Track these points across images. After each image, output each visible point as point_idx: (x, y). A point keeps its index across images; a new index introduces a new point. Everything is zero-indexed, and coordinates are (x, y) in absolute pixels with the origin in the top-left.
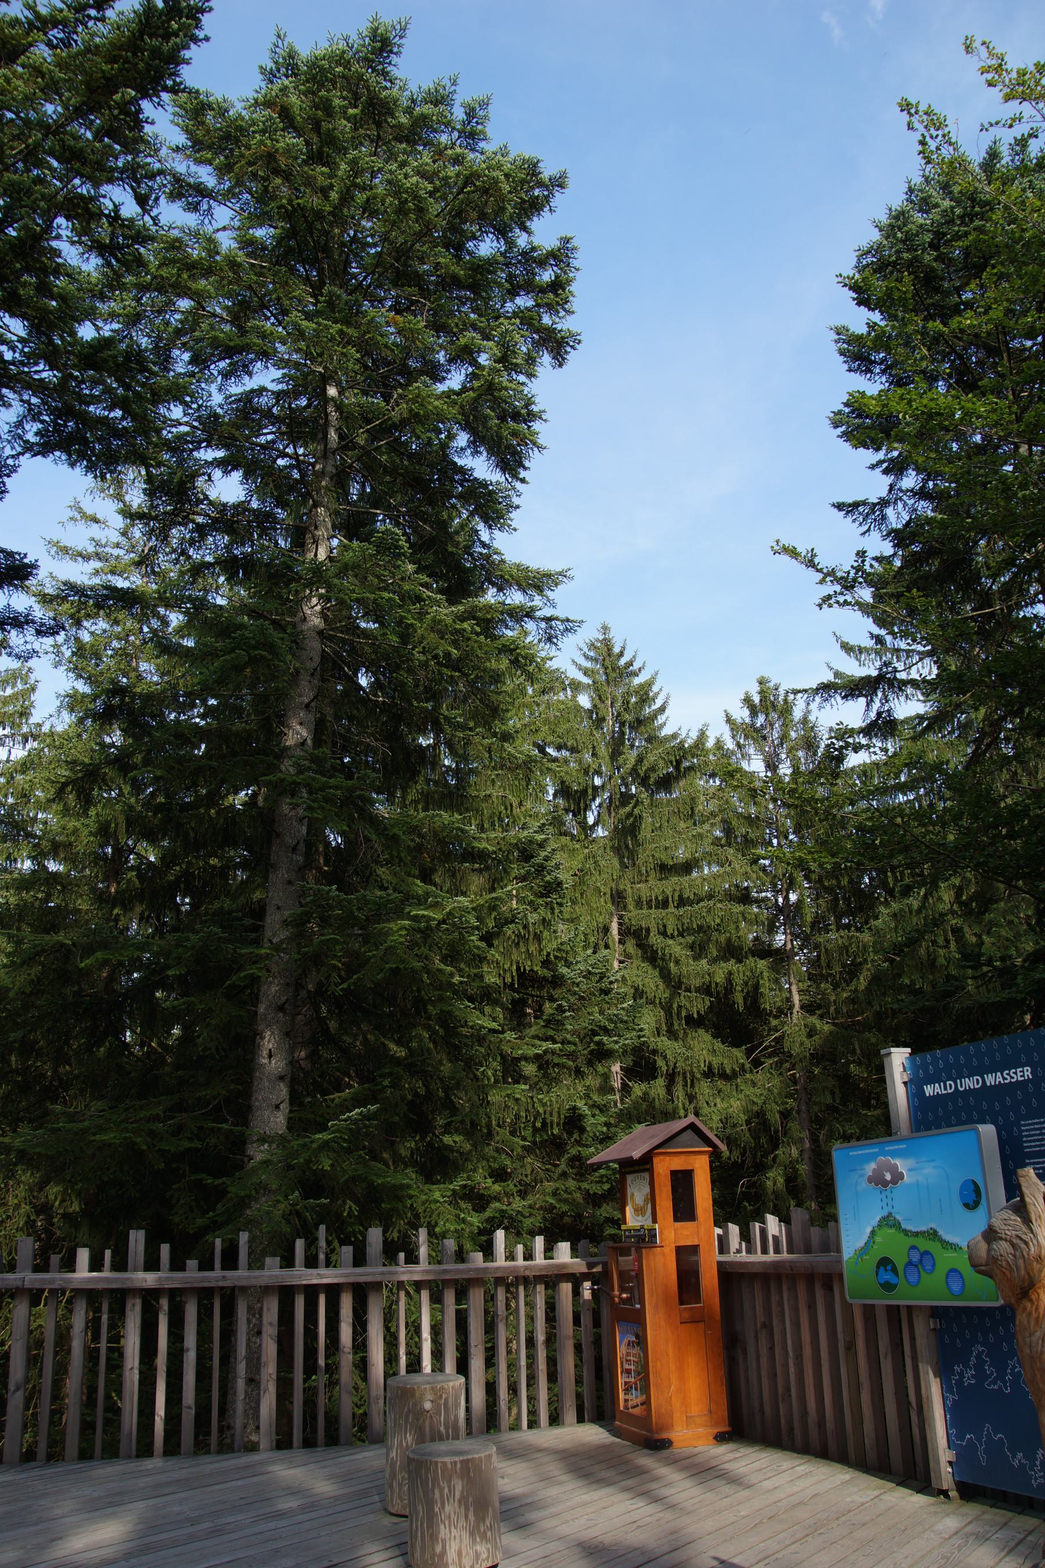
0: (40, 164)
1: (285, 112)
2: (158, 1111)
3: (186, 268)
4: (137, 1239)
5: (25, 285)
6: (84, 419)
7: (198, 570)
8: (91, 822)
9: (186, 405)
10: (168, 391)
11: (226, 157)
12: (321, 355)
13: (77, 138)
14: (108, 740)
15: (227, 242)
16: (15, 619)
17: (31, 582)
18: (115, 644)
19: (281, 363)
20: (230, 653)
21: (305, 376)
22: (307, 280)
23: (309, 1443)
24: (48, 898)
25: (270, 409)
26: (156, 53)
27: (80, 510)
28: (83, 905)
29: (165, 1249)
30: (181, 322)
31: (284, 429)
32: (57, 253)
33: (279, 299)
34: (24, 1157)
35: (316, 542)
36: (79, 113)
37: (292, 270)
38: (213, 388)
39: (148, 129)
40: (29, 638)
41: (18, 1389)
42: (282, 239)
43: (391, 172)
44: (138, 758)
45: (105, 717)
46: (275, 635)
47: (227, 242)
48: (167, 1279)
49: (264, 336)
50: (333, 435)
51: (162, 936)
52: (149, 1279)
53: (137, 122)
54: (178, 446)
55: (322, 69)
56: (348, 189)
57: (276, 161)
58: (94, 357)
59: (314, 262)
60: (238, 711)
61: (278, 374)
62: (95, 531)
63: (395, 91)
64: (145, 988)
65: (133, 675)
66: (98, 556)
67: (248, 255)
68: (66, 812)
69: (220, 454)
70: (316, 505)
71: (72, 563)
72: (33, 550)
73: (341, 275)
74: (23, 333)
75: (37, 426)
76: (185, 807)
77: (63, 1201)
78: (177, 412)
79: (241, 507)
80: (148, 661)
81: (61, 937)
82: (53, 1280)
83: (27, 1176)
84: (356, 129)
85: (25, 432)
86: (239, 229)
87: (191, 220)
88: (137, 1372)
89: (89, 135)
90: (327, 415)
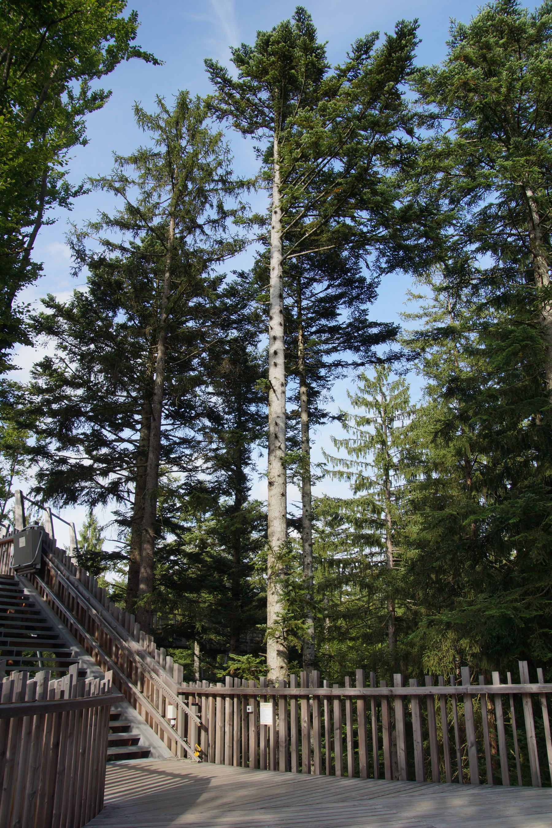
0: (357, 135)
1: (467, 59)
2: (516, 596)
3: (437, 156)
4: (523, 666)
5: (365, 194)
6: (407, 249)
7: (481, 308)
8: (452, 449)
9: (454, 225)
10: (445, 221)
11: (442, 95)
12: (518, 176)
13: (372, 116)
14: (451, 406)
15: (453, 137)
16: (395, 356)
17: (398, 337)
18: (445, 357)
19: (499, 188)
20: (510, 346)
21: (512, 190)
22: (500, 140)
23: (513, 782)
24: (437, 491)
25: (497, 214)
26: (400, 59)
27: (411, 294)
28: (454, 492)
29: (540, 671)
30: (440, 185)
31: (507, 222)
32: (377, 173)
33: (488, 155)
34: (448, 625)
35: (540, 276)
36: (369, 104)
37: (490, 137)
38: (465, 212)
39: (402, 97)
40: (404, 364)
41: (472, 746)
42: (481, 123)
43: (532, 64)
44: (471, 413)
45: (449, 395)
46: (533, 332)
47: (453, 137)
48: (544, 687)
49: (486, 177)
50: (535, 216)
51: (501, 503)
52: (534, 688)
53: (397, 95)
54: (455, 248)
55: (480, 28)
56: (510, 83)
57: (469, 85)
58: (406, 216)
59: (502, 128)
60: (516, 376)
61: (498, 194)
62: (421, 302)
63: (523, 19)
64: (497, 532)
65: (457, 370)
66: (426, 315)
67: (466, 139)
68: (436, 447)
69: (477, 245)
70: (535, 256)
71: (414, 322)
72: (396, 321)
73: (517, 130)
74: (368, 217)
75: (385, 259)
76: (498, 433)
77: (470, 647)
78: (451, 231)
79: (494, 270)
80: (463, 361)
81: (448, 511)
82: (482, 689)
83: (451, 635)
84: (506, 50)
85: (381, 263)
86: (457, 128)
87: (431, 133)
88: (534, 739)
89: (377, 112)
90: (530, 206)
